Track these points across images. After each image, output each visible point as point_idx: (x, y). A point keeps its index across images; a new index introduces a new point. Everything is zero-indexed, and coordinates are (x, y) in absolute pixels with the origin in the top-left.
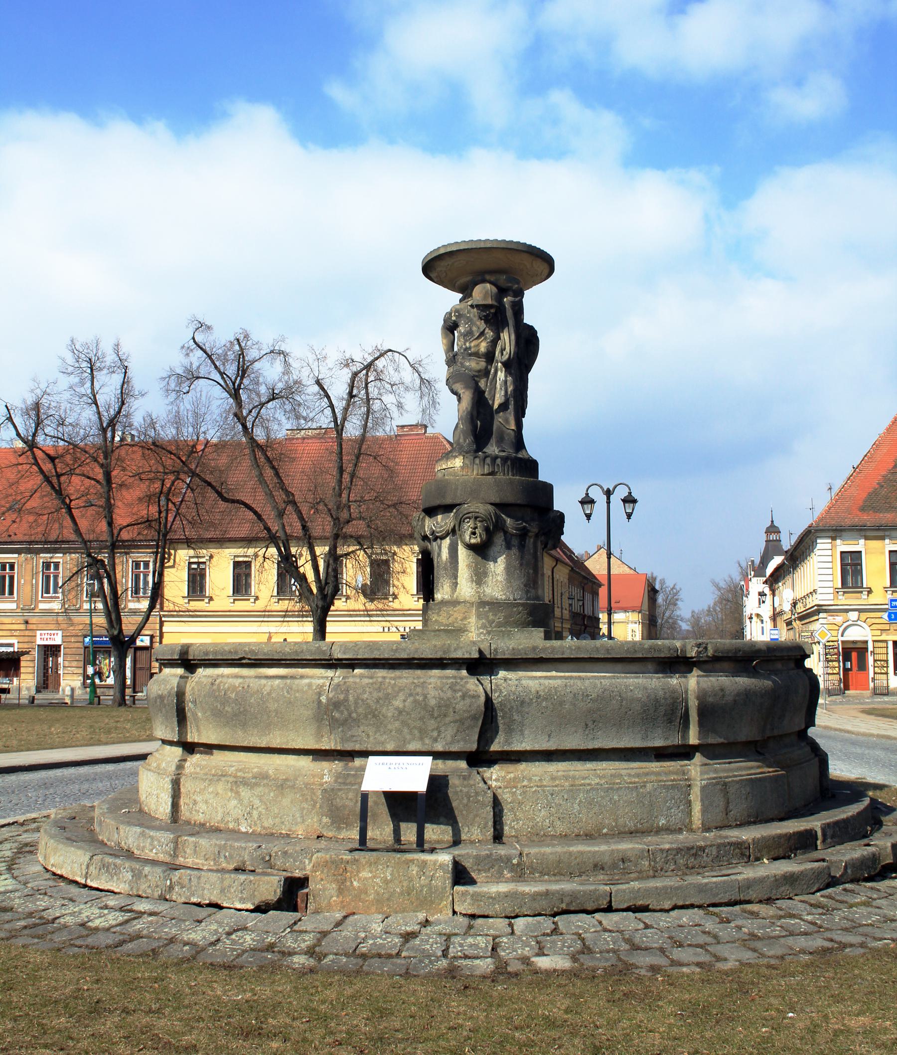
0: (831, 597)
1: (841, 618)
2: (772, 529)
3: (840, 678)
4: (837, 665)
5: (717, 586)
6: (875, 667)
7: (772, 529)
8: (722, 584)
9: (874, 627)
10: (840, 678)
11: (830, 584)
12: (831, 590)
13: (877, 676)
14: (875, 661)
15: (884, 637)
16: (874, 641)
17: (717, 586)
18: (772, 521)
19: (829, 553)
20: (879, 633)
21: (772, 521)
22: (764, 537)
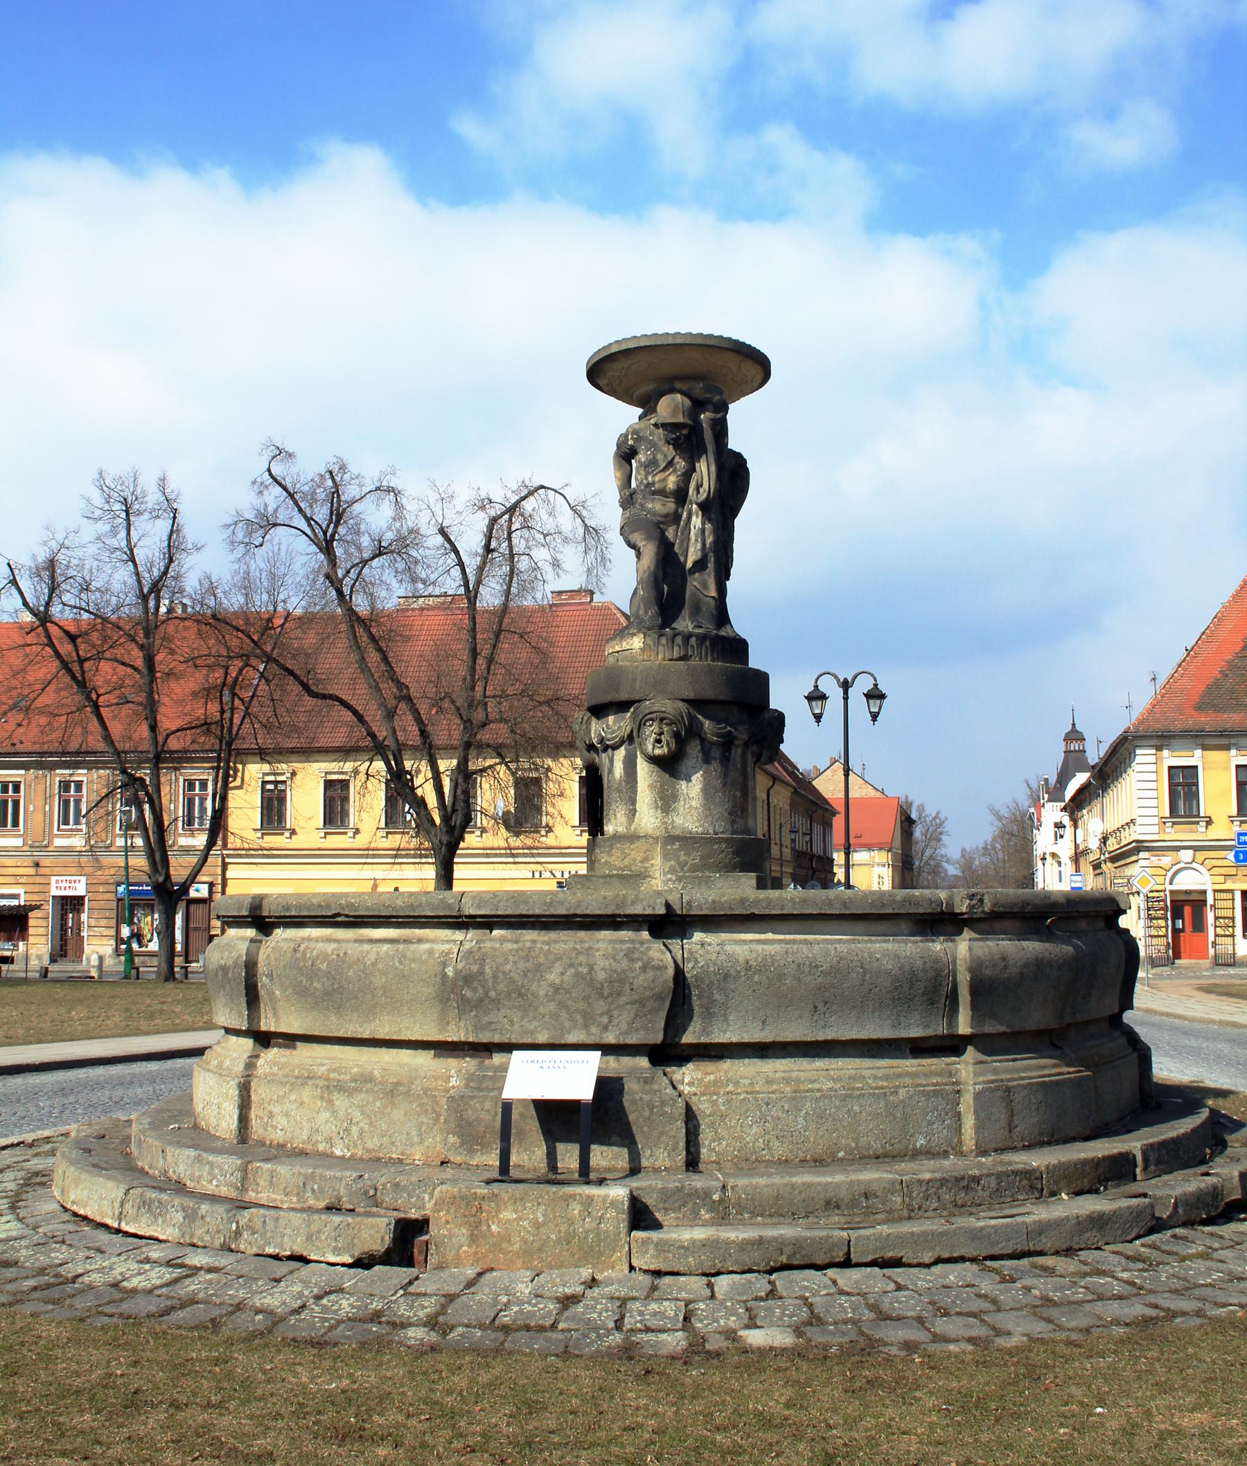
0: (1156, 829)
1: (1169, 858)
2: (1074, 735)
3: (1168, 943)
4: (1163, 925)
5: (997, 814)
6: (1216, 927)
7: (1074, 735)
8: (1004, 812)
9: (1215, 871)
10: (1168, 943)
11: (1154, 812)
12: (1156, 820)
13: (1219, 940)
14: (1216, 918)
15: (1229, 886)
16: (1215, 891)
17: (997, 814)
18: (1074, 725)
19: (1153, 768)
20: (1221, 879)
21: (1074, 725)
22: (1062, 747)
